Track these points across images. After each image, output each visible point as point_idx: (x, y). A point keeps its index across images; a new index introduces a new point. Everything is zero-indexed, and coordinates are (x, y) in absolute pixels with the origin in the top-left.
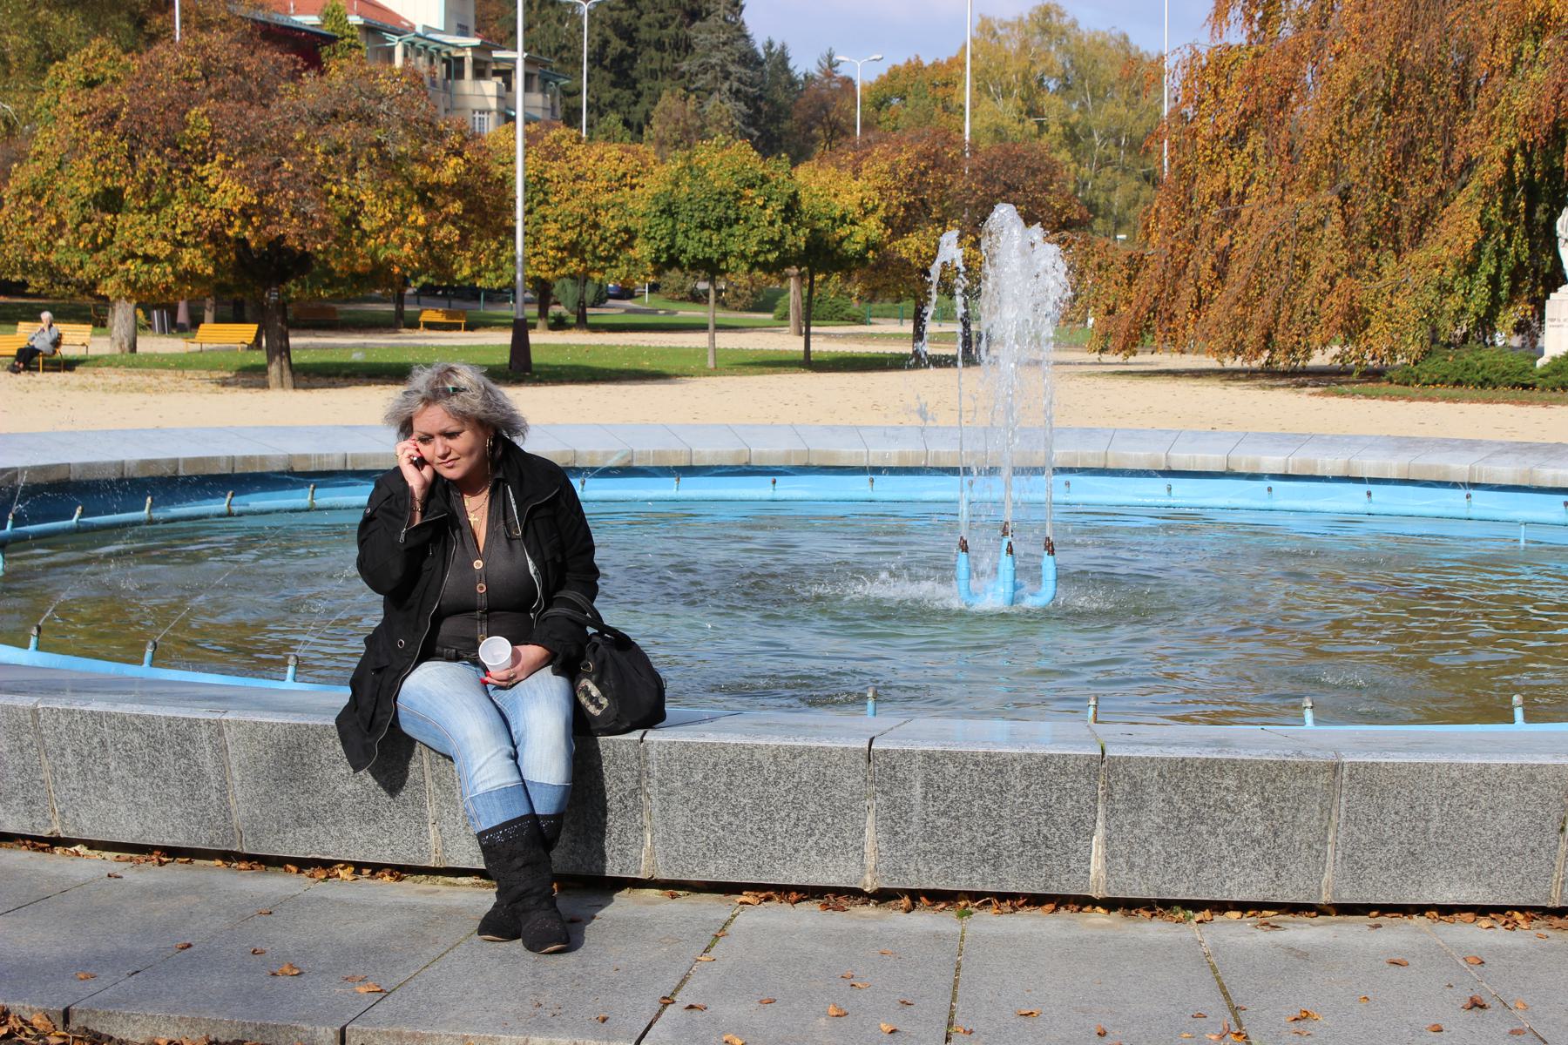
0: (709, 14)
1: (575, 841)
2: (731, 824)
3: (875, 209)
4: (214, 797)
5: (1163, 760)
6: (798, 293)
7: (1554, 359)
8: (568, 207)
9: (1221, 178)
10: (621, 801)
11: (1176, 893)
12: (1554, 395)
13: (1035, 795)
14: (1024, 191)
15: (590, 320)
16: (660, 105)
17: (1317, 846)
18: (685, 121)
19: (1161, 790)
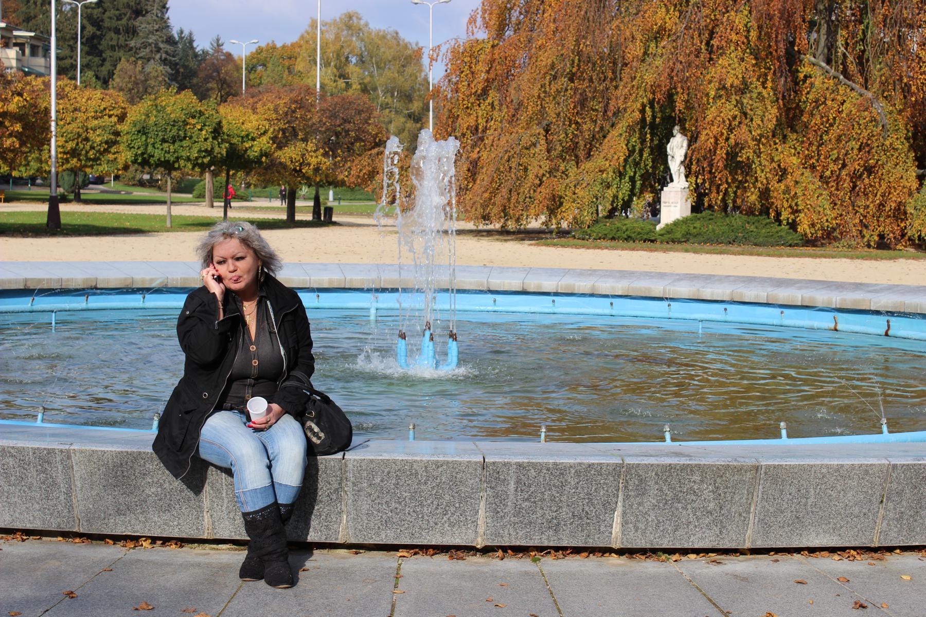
0: (147, 12)
1: (298, 521)
2: (396, 508)
3: (265, 132)
4: (62, 498)
5: (658, 465)
6: (211, 182)
7: (667, 225)
8: (70, 128)
9: (473, 117)
10: (328, 496)
11: (662, 544)
12: (669, 246)
13: (582, 488)
14: (354, 123)
15: (83, 197)
16: (119, 67)
17: (744, 515)
18: (135, 77)
19: (656, 483)
